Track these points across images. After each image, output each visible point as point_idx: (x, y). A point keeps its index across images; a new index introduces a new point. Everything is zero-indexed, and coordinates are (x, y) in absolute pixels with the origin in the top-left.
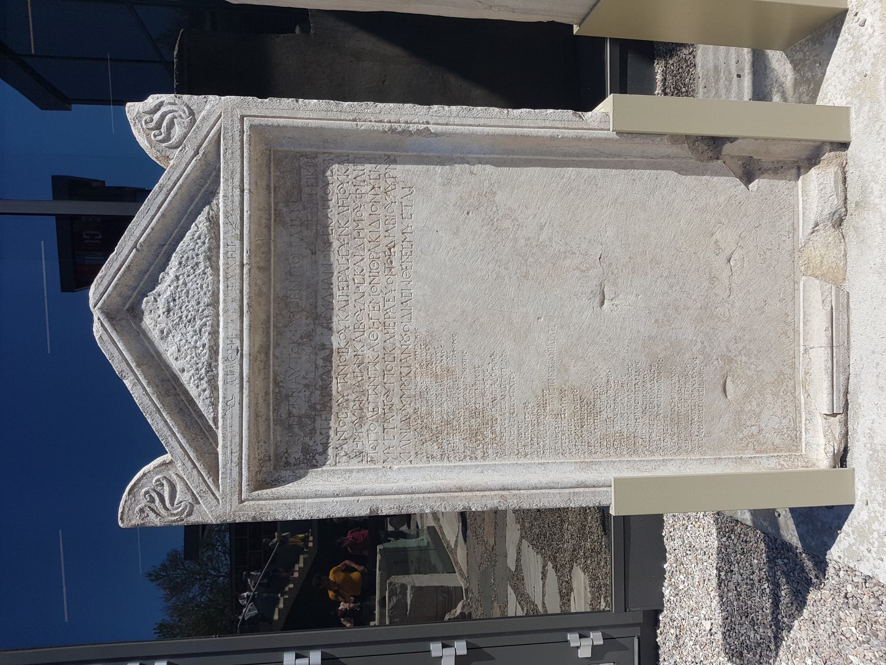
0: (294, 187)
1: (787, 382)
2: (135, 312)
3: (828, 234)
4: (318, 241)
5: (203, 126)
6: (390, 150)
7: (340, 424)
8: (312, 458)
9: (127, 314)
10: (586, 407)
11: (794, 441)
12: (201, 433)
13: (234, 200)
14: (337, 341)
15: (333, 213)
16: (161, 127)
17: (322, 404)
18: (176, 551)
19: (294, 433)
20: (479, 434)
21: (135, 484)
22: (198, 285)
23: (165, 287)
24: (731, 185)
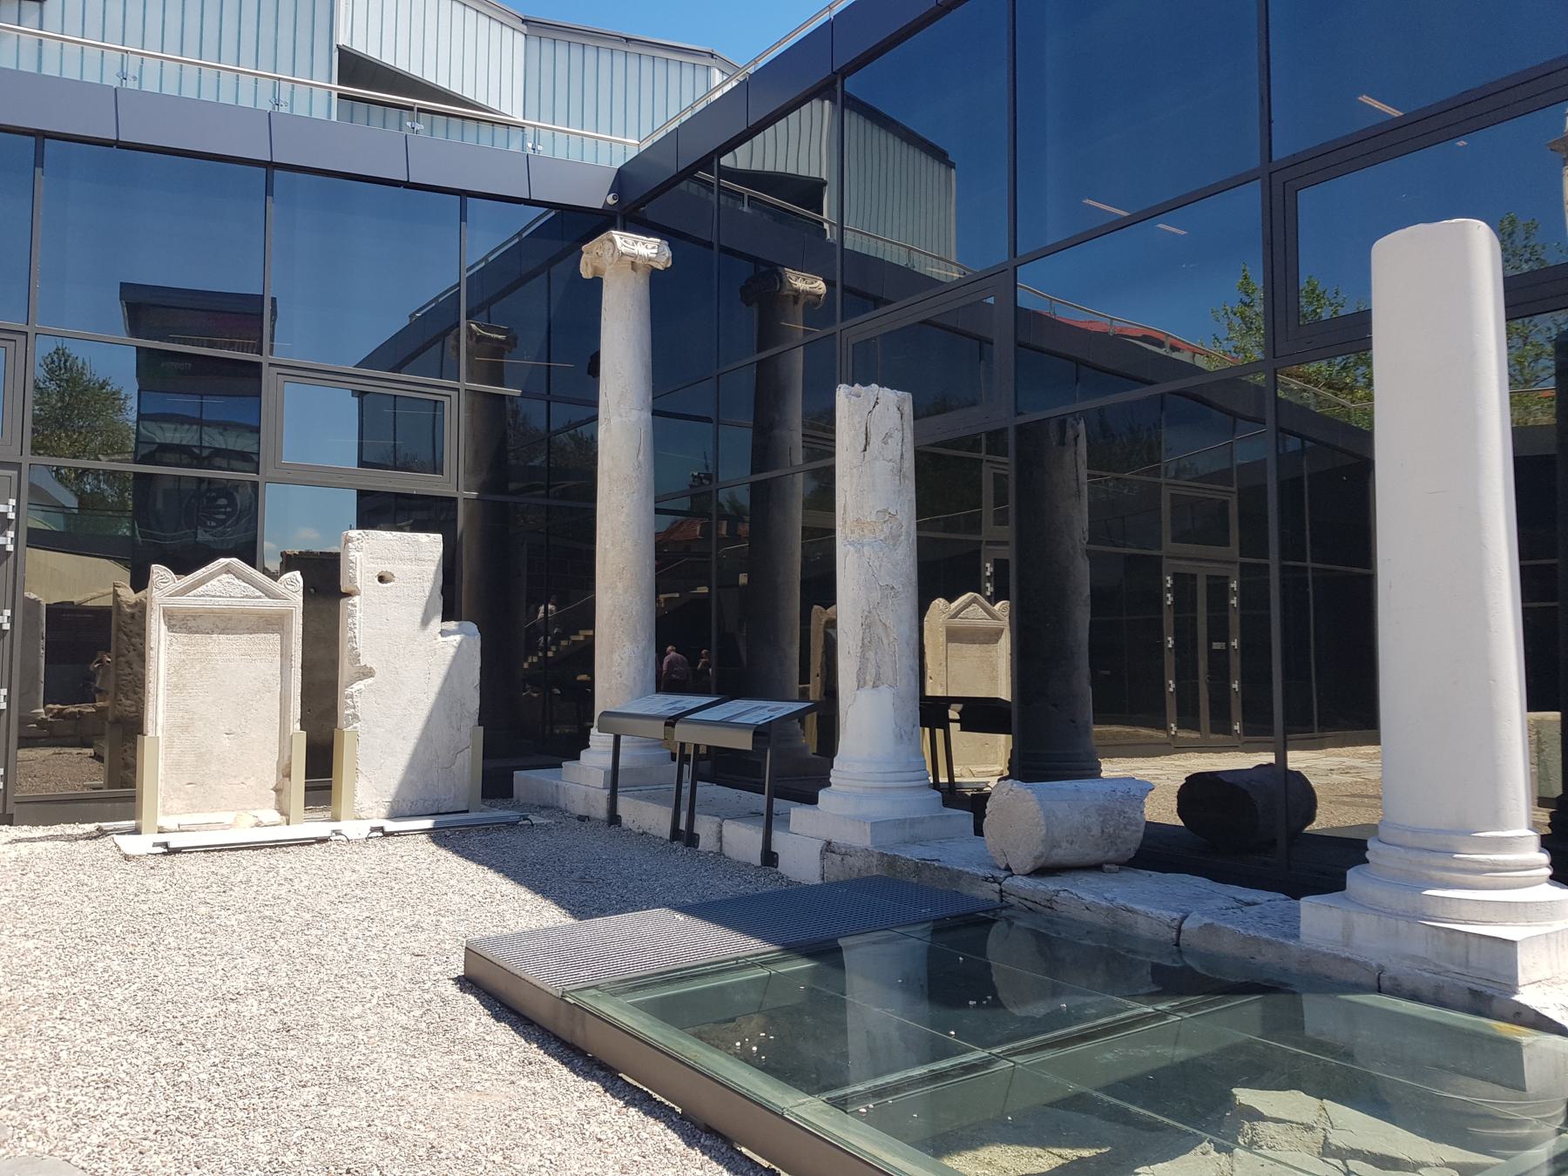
0: (272, 623)
1: (192, 808)
2: (228, 572)
3: (254, 821)
4: (251, 631)
5: (291, 595)
6: (285, 655)
7: (183, 637)
8: (171, 628)
9: (228, 570)
10: (185, 728)
11: (166, 814)
12: (184, 591)
13: (267, 604)
14: (215, 636)
15: (450, 855)
16: (292, 583)
17: (190, 631)
18: (1515, 993)
19: (180, 622)
20: (175, 688)
21: (1179, 1131)
22: (237, 592)
23: (237, 581)
24: (272, 782)
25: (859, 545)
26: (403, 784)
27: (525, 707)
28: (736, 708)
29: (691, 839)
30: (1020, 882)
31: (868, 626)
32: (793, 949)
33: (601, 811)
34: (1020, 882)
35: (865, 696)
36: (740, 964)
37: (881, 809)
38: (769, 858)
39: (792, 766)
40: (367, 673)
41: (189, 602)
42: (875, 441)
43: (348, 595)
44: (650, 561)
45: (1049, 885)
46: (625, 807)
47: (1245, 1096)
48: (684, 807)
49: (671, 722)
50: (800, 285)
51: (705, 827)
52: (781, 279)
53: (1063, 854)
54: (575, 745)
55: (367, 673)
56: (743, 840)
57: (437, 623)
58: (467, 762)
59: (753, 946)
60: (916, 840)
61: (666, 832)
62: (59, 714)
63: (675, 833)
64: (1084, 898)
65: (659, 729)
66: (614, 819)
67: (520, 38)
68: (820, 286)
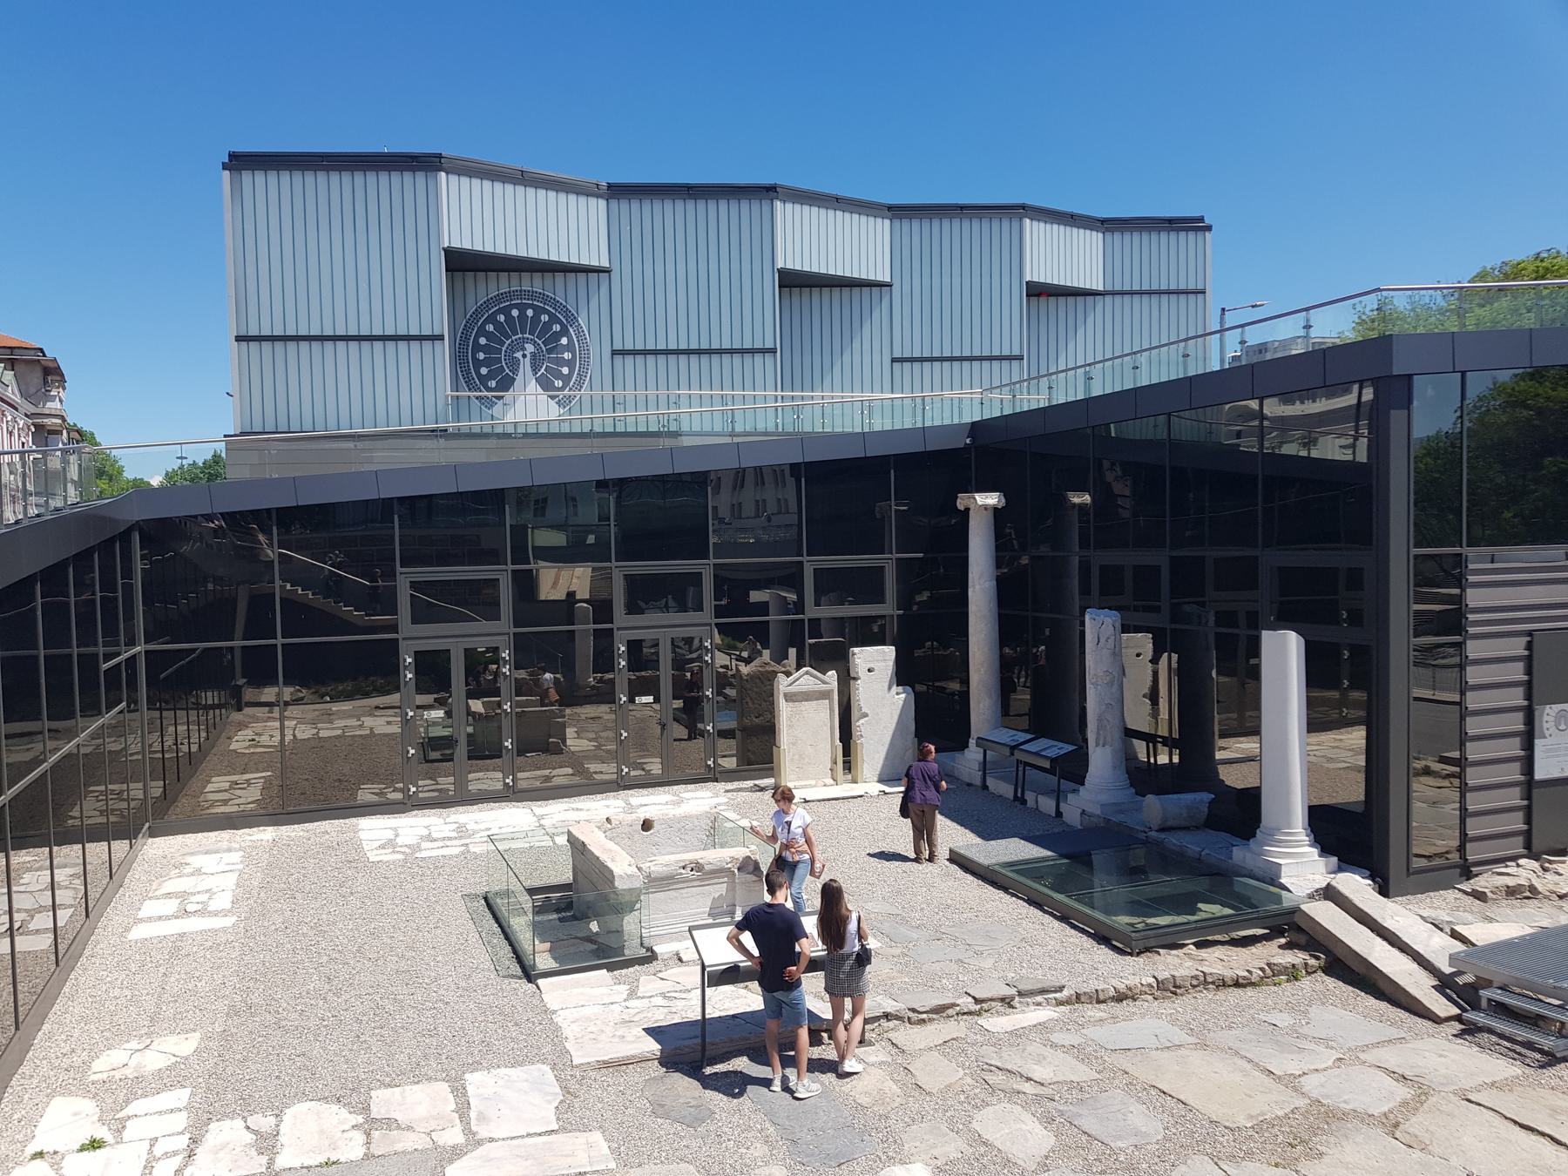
1: (799, 779)
6: (831, 709)
13: (823, 687)
19: (790, 698)
25: (1095, 685)
26: (884, 766)
27: (937, 718)
28: (1042, 743)
29: (1024, 802)
30: (1153, 834)
31: (1100, 720)
32: (1063, 856)
33: (978, 782)
34: (1153, 834)
35: (1099, 750)
36: (1044, 859)
37: (1104, 798)
38: (1059, 814)
39: (1073, 769)
40: (866, 715)
41: (793, 689)
42: (1102, 640)
43: (855, 679)
44: (997, 664)
45: (1163, 836)
46: (990, 782)
47: (1200, 905)
48: (1020, 784)
49: (1013, 748)
50: (1076, 500)
51: (1030, 797)
52: (1066, 499)
53: (1169, 824)
54: (964, 746)
55: (866, 715)
56: (1047, 804)
57: (894, 688)
58: (910, 755)
59: (1050, 853)
60: (1122, 812)
61: (1011, 795)
62: (601, 681)
63: (1016, 798)
64: (1173, 840)
65: (1007, 752)
66: (985, 787)
67: (887, 222)
68: (1087, 498)
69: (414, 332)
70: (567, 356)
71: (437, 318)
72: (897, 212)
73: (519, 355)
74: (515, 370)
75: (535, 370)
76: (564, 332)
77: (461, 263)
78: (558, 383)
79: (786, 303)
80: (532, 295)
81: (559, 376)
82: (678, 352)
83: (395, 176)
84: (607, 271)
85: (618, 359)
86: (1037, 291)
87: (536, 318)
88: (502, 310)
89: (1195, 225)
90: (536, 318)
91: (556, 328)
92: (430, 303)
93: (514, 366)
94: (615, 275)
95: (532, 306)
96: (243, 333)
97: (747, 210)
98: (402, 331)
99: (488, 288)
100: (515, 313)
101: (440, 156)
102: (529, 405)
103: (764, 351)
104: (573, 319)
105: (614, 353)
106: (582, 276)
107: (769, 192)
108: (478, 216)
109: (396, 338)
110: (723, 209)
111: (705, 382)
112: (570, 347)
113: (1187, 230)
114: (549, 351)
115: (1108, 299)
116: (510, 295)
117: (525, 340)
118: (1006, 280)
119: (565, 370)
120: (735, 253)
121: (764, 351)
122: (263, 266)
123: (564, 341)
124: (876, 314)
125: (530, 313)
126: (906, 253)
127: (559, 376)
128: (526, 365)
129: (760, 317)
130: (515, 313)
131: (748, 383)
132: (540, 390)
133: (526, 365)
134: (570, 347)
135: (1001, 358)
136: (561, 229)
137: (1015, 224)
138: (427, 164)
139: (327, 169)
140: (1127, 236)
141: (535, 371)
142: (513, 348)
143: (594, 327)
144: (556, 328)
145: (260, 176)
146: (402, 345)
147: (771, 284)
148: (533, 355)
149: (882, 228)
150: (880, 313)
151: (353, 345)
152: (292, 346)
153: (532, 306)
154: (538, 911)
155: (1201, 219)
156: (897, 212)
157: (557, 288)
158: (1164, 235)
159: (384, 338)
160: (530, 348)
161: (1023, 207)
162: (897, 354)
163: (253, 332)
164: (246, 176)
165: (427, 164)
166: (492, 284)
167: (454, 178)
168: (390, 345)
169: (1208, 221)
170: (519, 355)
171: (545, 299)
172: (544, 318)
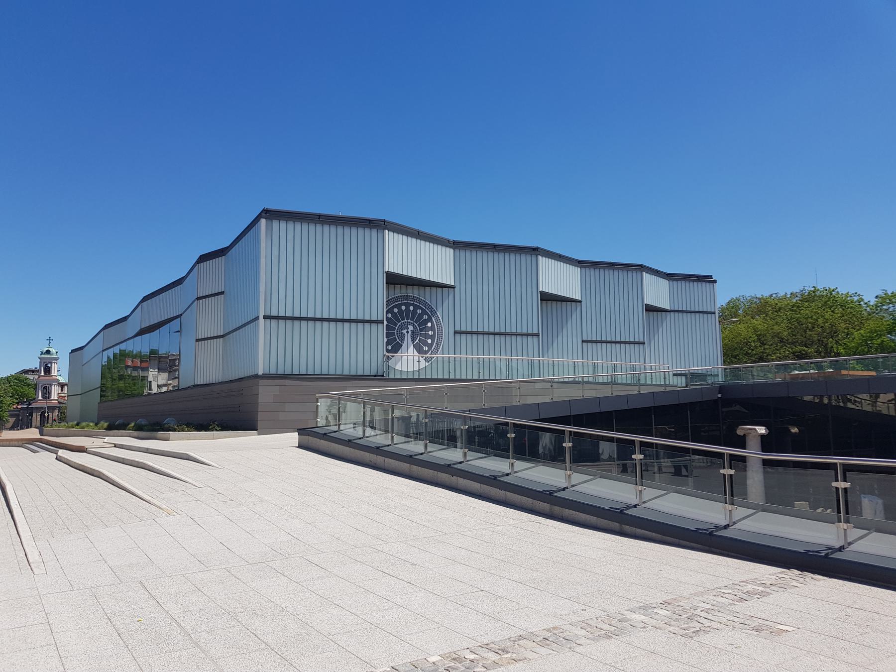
69: (325, 316)
70: (430, 333)
71: (380, 312)
72: (456, 245)
73: (405, 331)
74: (402, 340)
75: (413, 340)
76: (429, 319)
77: (393, 280)
78: (426, 348)
79: (544, 307)
80: (413, 298)
81: (426, 344)
82: (472, 333)
83: (361, 230)
84: (453, 287)
85: (458, 336)
86: (546, 298)
87: (415, 311)
88: (409, 305)
89: (707, 279)
90: (415, 311)
91: (426, 317)
92: (375, 302)
93: (402, 337)
94: (457, 290)
95: (403, 304)
96: (268, 314)
97: (525, 259)
98: (360, 317)
99: (399, 291)
100: (403, 308)
101: (384, 221)
102: (409, 361)
103: (533, 335)
104: (434, 313)
105: (456, 332)
106: (439, 289)
107: (535, 251)
108: (405, 256)
109: (357, 321)
110: (513, 259)
111: (469, 351)
112: (432, 328)
113: (702, 281)
114: (421, 330)
115: (672, 314)
116: (401, 298)
117: (408, 323)
118: (635, 302)
119: (429, 341)
120: (617, 292)
121: (533, 335)
122: (282, 276)
123: (429, 324)
124: (574, 316)
125: (411, 308)
126: (588, 286)
127: (426, 344)
128: (408, 337)
129: (530, 317)
130: (403, 308)
131: (486, 351)
132: (416, 353)
133: (408, 337)
134: (432, 328)
135: (634, 343)
136: (431, 263)
137: (639, 273)
138: (378, 225)
139: (681, 280)
140: (679, 283)
141: (413, 341)
142: (401, 328)
143: (446, 317)
144: (426, 317)
145: (283, 224)
146: (360, 325)
147: (536, 298)
148: (413, 332)
149: (449, 253)
150: (576, 316)
151: (332, 324)
152: (318, 323)
153: (403, 304)
154: (847, 521)
155: (711, 277)
156: (456, 245)
157: (426, 295)
158: (695, 284)
159: (350, 321)
160: (411, 328)
161: (641, 266)
162: (585, 339)
163: (274, 314)
164: (275, 223)
165: (378, 225)
166: (404, 290)
167: (391, 233)
168: (354, 325)
169: (714, 278)
170: (405, 331)
171: (420, 301)
172: (419, 311)
